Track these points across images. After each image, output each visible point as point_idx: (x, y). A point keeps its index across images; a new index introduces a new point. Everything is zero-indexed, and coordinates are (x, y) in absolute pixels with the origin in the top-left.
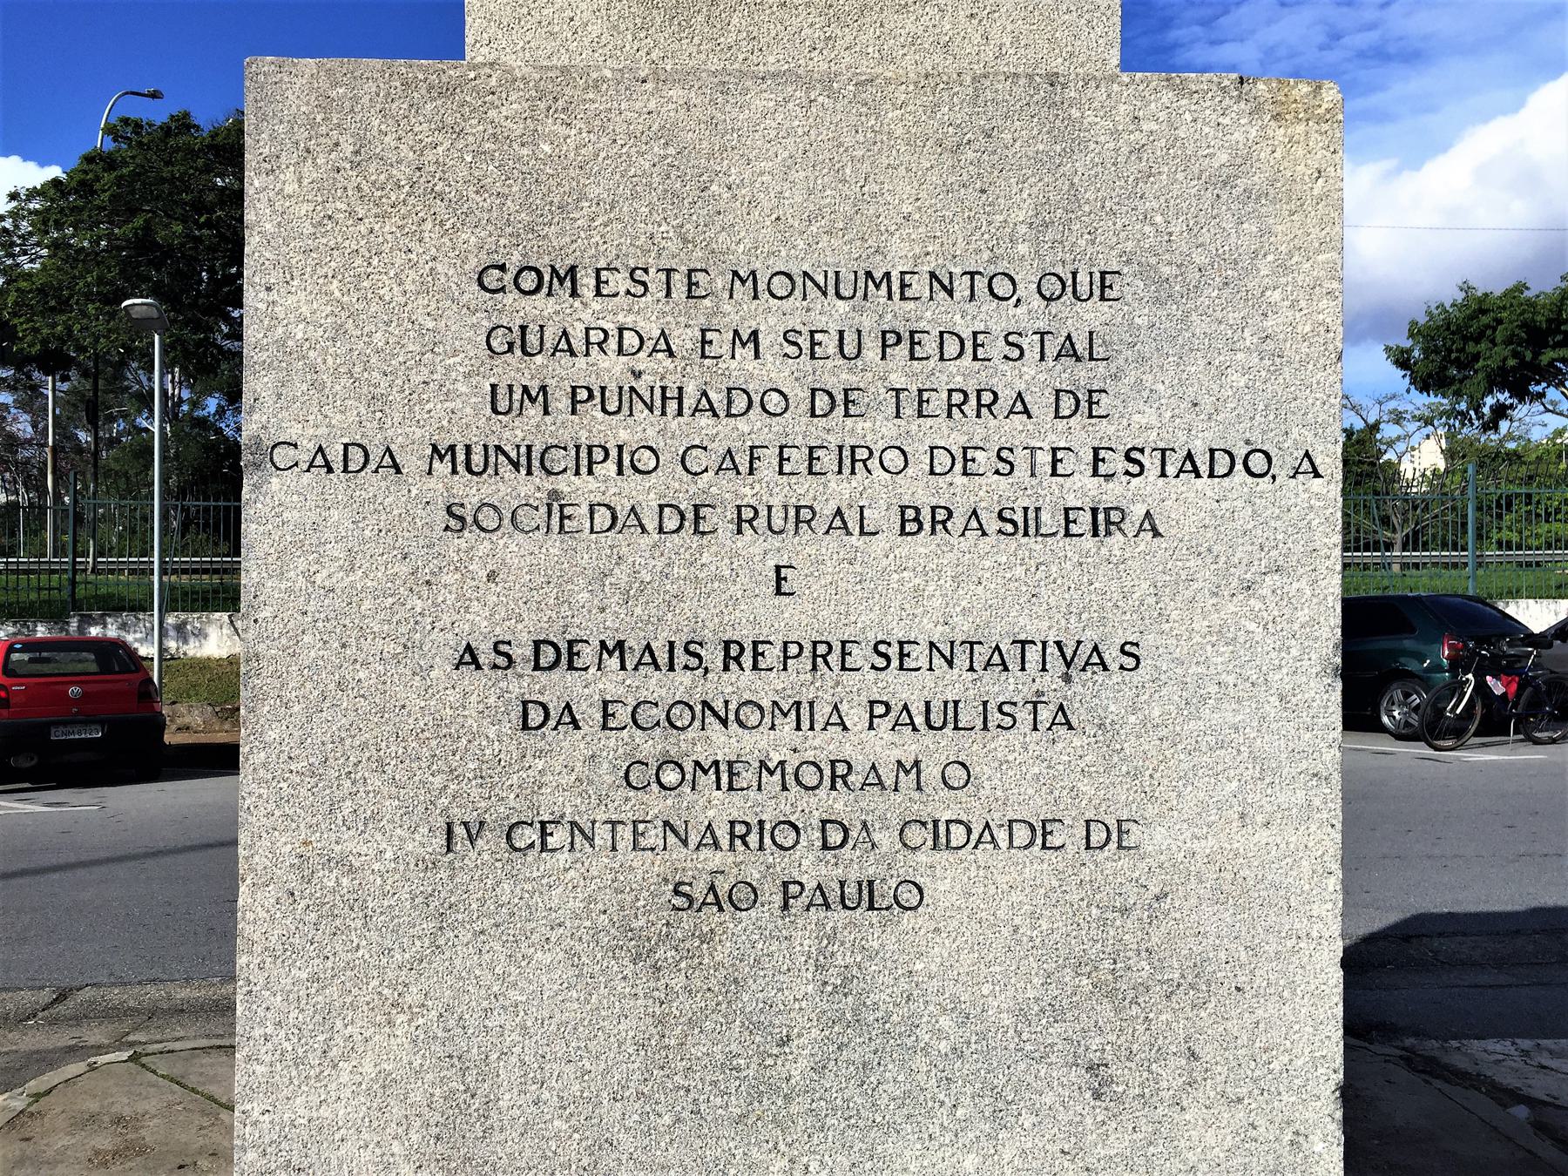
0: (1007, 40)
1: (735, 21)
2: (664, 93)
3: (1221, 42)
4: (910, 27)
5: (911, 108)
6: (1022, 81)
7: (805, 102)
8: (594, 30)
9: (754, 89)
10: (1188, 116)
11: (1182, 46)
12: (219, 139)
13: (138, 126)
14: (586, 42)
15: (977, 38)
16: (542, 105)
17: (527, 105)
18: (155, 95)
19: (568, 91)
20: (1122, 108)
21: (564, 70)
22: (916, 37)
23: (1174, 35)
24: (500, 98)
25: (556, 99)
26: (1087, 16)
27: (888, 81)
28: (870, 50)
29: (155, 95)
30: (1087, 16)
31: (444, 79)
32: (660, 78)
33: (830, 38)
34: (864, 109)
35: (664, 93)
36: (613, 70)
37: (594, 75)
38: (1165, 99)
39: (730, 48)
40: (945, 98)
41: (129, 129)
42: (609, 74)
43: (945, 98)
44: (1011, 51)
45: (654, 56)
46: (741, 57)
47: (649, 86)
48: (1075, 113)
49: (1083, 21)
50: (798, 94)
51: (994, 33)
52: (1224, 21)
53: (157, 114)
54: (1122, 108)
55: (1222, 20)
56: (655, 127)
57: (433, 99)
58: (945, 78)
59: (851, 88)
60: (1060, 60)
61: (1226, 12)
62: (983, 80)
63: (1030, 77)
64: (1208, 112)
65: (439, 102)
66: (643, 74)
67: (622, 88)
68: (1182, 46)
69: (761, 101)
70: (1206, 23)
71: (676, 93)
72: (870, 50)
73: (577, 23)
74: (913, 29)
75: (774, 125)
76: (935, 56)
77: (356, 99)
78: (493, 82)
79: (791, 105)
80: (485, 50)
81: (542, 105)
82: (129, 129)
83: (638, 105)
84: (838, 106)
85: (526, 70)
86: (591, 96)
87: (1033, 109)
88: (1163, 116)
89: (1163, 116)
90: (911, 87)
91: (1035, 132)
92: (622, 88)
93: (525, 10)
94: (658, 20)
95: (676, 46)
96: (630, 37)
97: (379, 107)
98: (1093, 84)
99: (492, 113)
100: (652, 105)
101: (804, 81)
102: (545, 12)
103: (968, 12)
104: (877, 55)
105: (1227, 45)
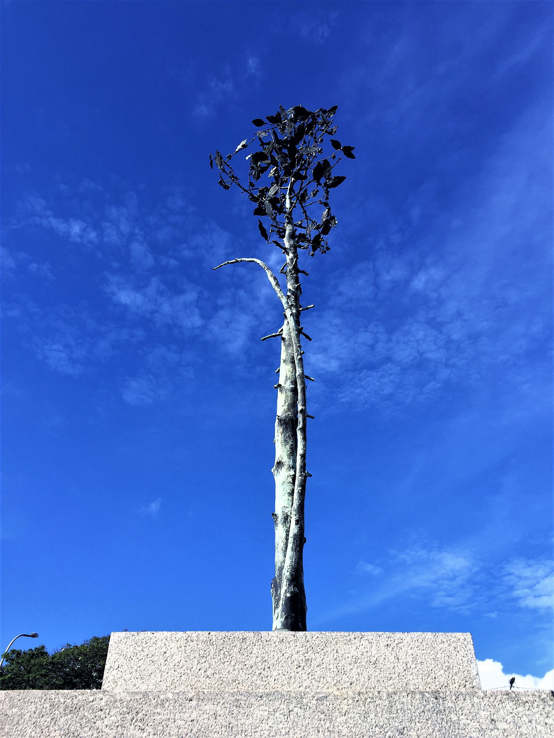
0: (410, 659)
1: (255, 651)
2: (202, 708)
3: (540, 596)
4: (354, 653)
5: (351, 715)
6: (418, 696)
7: (286, 712)
8: (177, 658)
9: (256, 704)
10: (525, 718)
11: (521, 598)
12: (56, 659)
13: (19, 654)
14: (172, 665)
15: (392, 659)
16: (129, 717)
17: (119, 717)
18: (34, 636)
19: (145, 708)
20: (482, 713)
21: (145, 694)
22: (357, 659)
23: (516, 593)
24: (105, 713)
25: (137, 713)
26: (454, 645)
27: (336, 698)
28: (331, 666)
29: (34, 636)
30: (454, 645)
31: (75, 702)
32: (201, 698)
33: (308, 660)
34: (322, 716)
35: (202, 708)
36: (173, 693)
37: (162, 697)
38: (508, 707)
39: (251, 667)
40: (372, 708)
41: (14, 656)
42: (170, 696)
43: (372, 708)
44: (413, 666)
45: (208, 673)
46: (258, 672)
47: (194, 703)
48: (454, 717)
49: (452, 648)
50: (282, 706)
51: (401, 655)
52: (538, 586)
53: (27, 645)
54: (482, 713)
55: (537, 585)
56: (195, 730)
57: (66, 715)
58: (370, 695)
59: (314, 702)
60: (442, 671)
61: (538, 582)
62: (393, 696)
63: (422, 693)
64: (537, 715)
65: (69, 717)
66: (190, 696)
67: (177, 704)
68: (521, 598)
69: (260, 711)
70: (531, 587)
71: (209, 707)
72: (331, 666)
73: (167, 655)
74: (355, 654)
75: (267, 727)
76: (369, 670)
77: (21, 716)
78: (103, 703)
79: (277, 714)
80: (115, 672)
81: (129, 717)
82: (14, 656)
83: (187, 715)
84: (307, 714)
85: (123, 695)
86: (158, 710)
87: (427, 715)
88: (509, 718)
89: (509, 718)
90: (351, 701)
91: (431, 730)
92: (177, 704)
93: (140, 648)
94: (212, 652)
95: (222, 666)
96: (196, 662)
97: (34, 720)
98: (461, 697)
99: (99, 723)
100: (194, 716)
101: (286, 698)
102: (151, 649)
103: (386, 643)
104: (335, 670)
105: (542, 598)
